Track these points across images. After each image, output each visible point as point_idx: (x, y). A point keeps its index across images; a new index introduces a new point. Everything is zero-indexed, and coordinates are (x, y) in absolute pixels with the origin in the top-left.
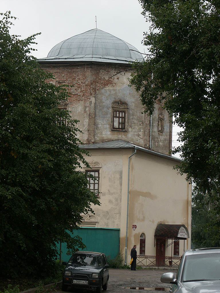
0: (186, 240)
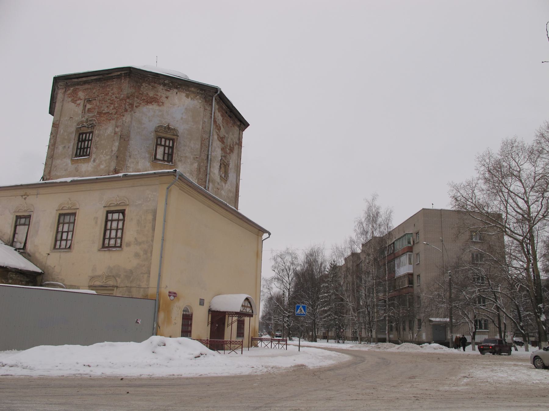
0: (252, 318)
